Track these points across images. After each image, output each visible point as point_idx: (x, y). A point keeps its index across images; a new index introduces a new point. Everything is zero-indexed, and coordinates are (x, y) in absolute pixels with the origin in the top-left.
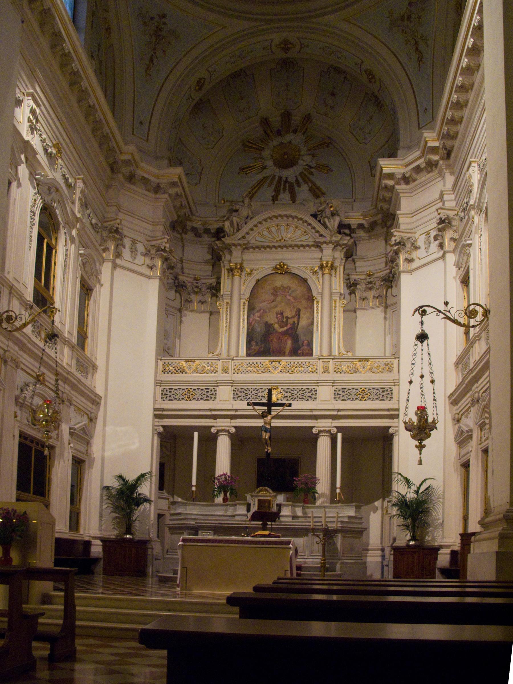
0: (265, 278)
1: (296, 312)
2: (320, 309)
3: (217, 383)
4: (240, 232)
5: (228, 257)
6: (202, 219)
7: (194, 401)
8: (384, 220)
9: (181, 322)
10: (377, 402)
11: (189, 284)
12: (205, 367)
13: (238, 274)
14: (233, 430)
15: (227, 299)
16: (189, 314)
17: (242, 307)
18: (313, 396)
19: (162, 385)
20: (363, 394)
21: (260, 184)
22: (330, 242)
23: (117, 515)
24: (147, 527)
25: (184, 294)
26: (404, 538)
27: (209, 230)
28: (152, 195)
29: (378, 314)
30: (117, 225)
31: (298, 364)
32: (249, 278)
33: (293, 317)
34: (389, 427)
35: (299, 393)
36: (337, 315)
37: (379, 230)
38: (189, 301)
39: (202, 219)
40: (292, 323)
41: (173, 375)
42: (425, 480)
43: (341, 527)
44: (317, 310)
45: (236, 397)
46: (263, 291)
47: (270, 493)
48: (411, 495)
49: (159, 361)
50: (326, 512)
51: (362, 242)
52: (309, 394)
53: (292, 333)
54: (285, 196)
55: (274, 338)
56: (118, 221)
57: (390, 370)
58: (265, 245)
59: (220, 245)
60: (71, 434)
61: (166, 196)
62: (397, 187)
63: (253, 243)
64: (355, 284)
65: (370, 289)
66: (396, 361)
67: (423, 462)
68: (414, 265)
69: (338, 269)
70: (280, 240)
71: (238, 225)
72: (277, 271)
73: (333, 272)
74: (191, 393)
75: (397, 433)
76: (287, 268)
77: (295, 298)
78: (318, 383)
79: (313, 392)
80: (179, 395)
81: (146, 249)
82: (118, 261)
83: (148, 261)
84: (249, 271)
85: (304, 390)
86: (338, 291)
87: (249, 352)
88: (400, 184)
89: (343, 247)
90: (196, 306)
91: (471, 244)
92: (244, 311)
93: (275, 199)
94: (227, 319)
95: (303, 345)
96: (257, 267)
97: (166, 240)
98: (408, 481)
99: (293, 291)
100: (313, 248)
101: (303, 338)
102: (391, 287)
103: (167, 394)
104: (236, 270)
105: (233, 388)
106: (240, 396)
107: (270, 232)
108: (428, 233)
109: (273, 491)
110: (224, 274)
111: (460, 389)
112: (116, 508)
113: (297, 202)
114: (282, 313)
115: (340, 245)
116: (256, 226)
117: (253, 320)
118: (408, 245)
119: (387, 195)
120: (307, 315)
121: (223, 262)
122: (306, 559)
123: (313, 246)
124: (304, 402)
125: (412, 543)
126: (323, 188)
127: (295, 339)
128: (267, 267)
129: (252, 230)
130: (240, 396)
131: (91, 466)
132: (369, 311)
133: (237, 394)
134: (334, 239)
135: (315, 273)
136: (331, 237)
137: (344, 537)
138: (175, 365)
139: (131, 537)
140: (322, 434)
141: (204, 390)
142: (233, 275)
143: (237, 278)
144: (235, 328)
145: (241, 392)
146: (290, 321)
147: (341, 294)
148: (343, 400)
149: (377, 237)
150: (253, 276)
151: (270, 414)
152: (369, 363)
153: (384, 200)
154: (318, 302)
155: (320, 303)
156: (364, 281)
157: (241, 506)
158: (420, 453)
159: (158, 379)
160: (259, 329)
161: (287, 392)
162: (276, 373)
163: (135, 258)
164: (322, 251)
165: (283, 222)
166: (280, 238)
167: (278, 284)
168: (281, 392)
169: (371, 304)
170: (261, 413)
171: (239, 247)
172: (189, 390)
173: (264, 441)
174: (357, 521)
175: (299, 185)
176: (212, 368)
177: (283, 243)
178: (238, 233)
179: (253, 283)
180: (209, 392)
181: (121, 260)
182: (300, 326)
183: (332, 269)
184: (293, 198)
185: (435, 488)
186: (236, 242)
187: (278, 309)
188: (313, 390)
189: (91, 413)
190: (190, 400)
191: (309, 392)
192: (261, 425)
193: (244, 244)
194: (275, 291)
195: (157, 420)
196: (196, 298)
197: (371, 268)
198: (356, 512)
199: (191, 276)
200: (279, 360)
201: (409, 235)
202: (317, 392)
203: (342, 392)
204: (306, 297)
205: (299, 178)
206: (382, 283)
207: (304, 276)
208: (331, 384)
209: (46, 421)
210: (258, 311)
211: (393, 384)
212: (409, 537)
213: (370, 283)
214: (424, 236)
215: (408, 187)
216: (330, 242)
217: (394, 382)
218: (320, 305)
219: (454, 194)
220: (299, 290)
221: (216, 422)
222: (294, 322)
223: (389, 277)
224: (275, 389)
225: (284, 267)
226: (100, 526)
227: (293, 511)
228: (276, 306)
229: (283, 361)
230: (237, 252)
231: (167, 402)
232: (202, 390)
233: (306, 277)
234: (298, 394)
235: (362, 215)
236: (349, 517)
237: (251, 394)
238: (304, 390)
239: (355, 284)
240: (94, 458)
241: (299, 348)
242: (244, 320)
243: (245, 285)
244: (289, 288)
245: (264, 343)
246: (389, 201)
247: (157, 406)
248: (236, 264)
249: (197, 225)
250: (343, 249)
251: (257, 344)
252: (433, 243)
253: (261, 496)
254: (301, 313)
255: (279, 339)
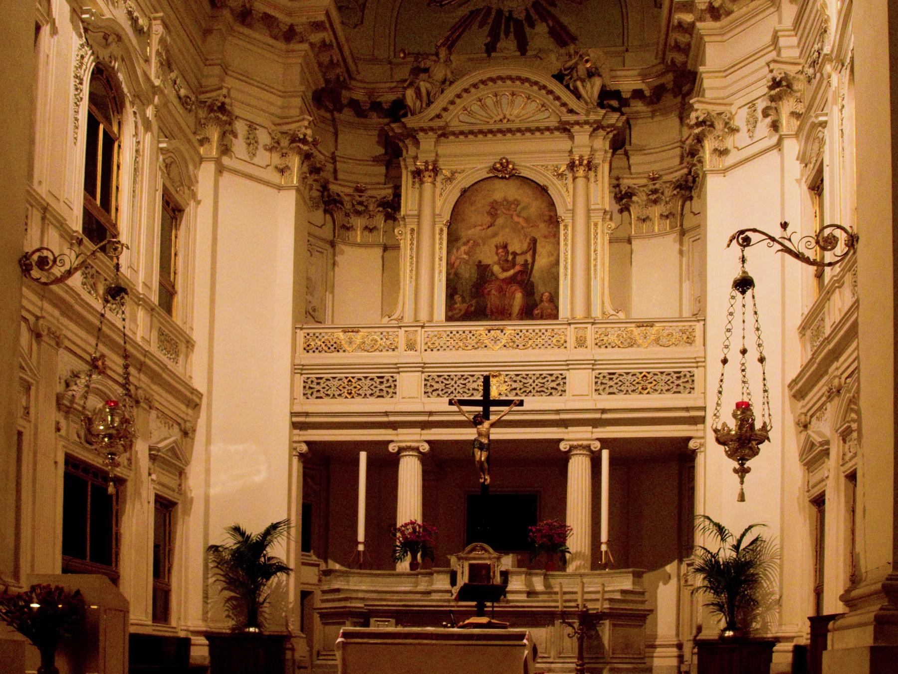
0: (476, 187)
1: (529, 244)
2: (569, 237)
3: (398, 368)
4: (432, 106)
5: (412, 151)
6: (366, 85)
7: (358, 400)
8: (678, 82)
9: (334, 264)
10: (669, 395)
11: (347, 199)
12: (377, 341)
13: (430, 180)
14: (425, 448)
15: (412, 224)
16: (347, 249)
17: (437, 237)
18: (560, 388)
19: (304, 372)
20: (644, 382)
21: (465, 24)
22: (586, 122)
23: (233, 594)
24: (284, 614)
25: (339, 216)
26: (715, 626)
27: (380, 103)
28: (281, 45)
29: (668, 245)
30: (222, 99)
31: (534, 334)
32: (450, 187)
33: (523, 253)
34: (689, 439)
35: (537, 382)
36: (599, 248)
37: (669, 100)
38: (347, 228)
39: (366, 85)
40: (522, 262)
41: (323, 354)
42: (750, 527)
43: (610, 608)
44: (566, 239)
45: (430, 390)
46: (473, 208)
47: (489, 553)
48: (726, 554)
49: (298, 331)
50: (584, 583)
51: (640, 121)
52: (554, 385)
53: (524, 279)
54: (508, 44)
55: (492, 290)
56: (225, 91)
57: (690, 341)
58: (475, 128)
59: (398, 131)
60: (153, 458)
61: (305, 46)
62: (699, 25)
63: (455, 125)
64: (629, 195)
65: (655, 202)
66: (699, 326)
67: (746, 498)
68: (729, 160)
69: (600, 169)
70: (501, 120)
71: (428, 94)
72: (497, 173)
73: (592, 174)
74: (354, 385)
75: (702, 449)
76: (514, 169)
77: (527, 220)
78: (568, 365)
79: (560, 381)
80: (334, 388)
81: (273, 138)
82: (226, 160)
83: (276, 159)
84: (448, 174)
85: (545, 378)
86: (600, 207)
87: (450, 314)
88: (704, 21)
89: (609, 130)
90: (359, 236)
91: (826, 122)
92: (441, 243)
93: (490, 48)
94: (412, 258)
95: (542, 301)
96: (462, 167)
97: (306, 123)
98: (721, 530)
99: (524, 208)
100: (557, 133)
101: (542, 289)
102: (691, 198)
103: (314, 385)
104: (427, 174)
105: (424, 376)
106: (437, 390)
107: (483, 106)
108: (752, 104)
109: (495, 550)
110: (406, 179)
111: (808, 371)
112: (231, 583)
113: (529, 53)
114: (505, 247)
115: (603, 128)
116: (459, 96)
117: (457, 258)
118: (719, 125)
119: (683, 39)
120: (549, 248)
121: (404, 160)
122: (552, 663)
123: (557, 129)
124: (544, 398)
125: (729, 633)
126: (573, 29)
127: (529, 290)
128: (479, 166)
129: (453, 103)
130: (437, 390)
131: (187, 512)
132: (654, 241)
133: (432, 386)
134: (592, 117)
135: (561, 176)
136: (587, 114)
137: (614, 625)
138: (326, 337)
139: (257, 630)
140: (575, 452)
141: (376, 379)
142: (422, 182)
143: (428, 186)
144: (425, 271)
145: (437, 382)
146: (520, 260)
147: (605, 212)
148: (610, 393)
149: (665, 112)
150: (455, 182)
151: (488, 419)
152: (653, 330)
153: (677, 47)
154: (566, 226)
155: (570, 228)
156: (645, 189)
157: (441, 576)
158: (742, 482)
159: (297, 362)
160: (468, 273)
161: (515, 381)
162: (497, 348)
163: (254, 155)
164: (572, 138)
165: (505, 88)
166: (501, 117)
167: (498, 196)
168: (505, 382)
169: (656, 228)
170: (471, 417)
171: (431, 133)
172: (350, 381)
173: (478, 466)
174: (636, 598)
175: (532, 25)
176: (388, 342)
177: (505, 126)
178: (429, 110)
179: (456, 195)
180: (383, 383)
181: (231, 157)
182: (536, 267)
183: (590, 169)
184: (523, 47)
185: (767, 540)
186: (425, 125)
187: (499, 240)
188: (560, 377)
189: (185, 421)
190: (353, 397)
191: (553, 381)
192: (472, 437)
193: (440, 128)
194: (493, 208)
195: (297, 431)
196: (359, 222)
197: (656, 167)
198: (634, 583)
199: (349, 184)
200: (501, 327)
201: (720, 109)
202: (567, 381)
203: (608, 380)
204: (547, 218)
205: (532, 12)
206: (675, 192)
207: (541, 181)
208: (591, 366)
209: (110, 436)
210: (465, 244)
211: (695, 365)
212: (723, 624)
213: (655, 192)
214: (745, 110)
215: (718, 24)
216: (586, 122)
217: (697, 362)
218: (570, 232)
219: (796, 35)
220: (535, 206)
221: (397, 435)
222: (526, 261)
223: (686, 181)
224: (496, 376)
225: (507, 166)
226: (205, 613)
227: (529, 584)
228: (495, 235)
229: (509, 328)
230: (427, 142)
231: (313, 400)
232: (372, 379)
233: (546, 183)
234: (534, 385)
235: (639, 75)
236: (623, 592)
237: (456, 386)
238: (545, 378)
239: (629, 195)
240: (192, 499)
241: (535, 306)
242: (441, 259)
243: (442, 199)
244: (517, 203)
245: (474, 298)
246: (685, 50)
247: (297, 409)
248: (427, 163)
249: (359, 95)
250: (608, 133)
251: (464, 301)
252: (762, 121)
253: (474, 559)
254: (538, 245)
255: (501, 290)
